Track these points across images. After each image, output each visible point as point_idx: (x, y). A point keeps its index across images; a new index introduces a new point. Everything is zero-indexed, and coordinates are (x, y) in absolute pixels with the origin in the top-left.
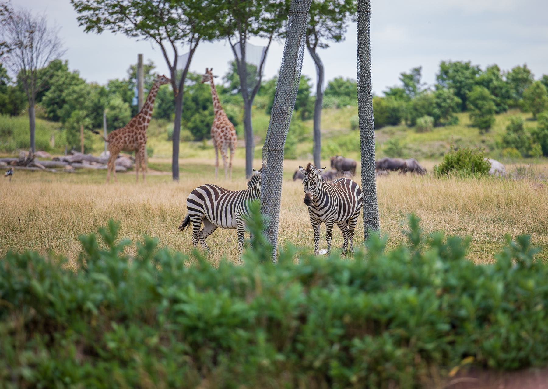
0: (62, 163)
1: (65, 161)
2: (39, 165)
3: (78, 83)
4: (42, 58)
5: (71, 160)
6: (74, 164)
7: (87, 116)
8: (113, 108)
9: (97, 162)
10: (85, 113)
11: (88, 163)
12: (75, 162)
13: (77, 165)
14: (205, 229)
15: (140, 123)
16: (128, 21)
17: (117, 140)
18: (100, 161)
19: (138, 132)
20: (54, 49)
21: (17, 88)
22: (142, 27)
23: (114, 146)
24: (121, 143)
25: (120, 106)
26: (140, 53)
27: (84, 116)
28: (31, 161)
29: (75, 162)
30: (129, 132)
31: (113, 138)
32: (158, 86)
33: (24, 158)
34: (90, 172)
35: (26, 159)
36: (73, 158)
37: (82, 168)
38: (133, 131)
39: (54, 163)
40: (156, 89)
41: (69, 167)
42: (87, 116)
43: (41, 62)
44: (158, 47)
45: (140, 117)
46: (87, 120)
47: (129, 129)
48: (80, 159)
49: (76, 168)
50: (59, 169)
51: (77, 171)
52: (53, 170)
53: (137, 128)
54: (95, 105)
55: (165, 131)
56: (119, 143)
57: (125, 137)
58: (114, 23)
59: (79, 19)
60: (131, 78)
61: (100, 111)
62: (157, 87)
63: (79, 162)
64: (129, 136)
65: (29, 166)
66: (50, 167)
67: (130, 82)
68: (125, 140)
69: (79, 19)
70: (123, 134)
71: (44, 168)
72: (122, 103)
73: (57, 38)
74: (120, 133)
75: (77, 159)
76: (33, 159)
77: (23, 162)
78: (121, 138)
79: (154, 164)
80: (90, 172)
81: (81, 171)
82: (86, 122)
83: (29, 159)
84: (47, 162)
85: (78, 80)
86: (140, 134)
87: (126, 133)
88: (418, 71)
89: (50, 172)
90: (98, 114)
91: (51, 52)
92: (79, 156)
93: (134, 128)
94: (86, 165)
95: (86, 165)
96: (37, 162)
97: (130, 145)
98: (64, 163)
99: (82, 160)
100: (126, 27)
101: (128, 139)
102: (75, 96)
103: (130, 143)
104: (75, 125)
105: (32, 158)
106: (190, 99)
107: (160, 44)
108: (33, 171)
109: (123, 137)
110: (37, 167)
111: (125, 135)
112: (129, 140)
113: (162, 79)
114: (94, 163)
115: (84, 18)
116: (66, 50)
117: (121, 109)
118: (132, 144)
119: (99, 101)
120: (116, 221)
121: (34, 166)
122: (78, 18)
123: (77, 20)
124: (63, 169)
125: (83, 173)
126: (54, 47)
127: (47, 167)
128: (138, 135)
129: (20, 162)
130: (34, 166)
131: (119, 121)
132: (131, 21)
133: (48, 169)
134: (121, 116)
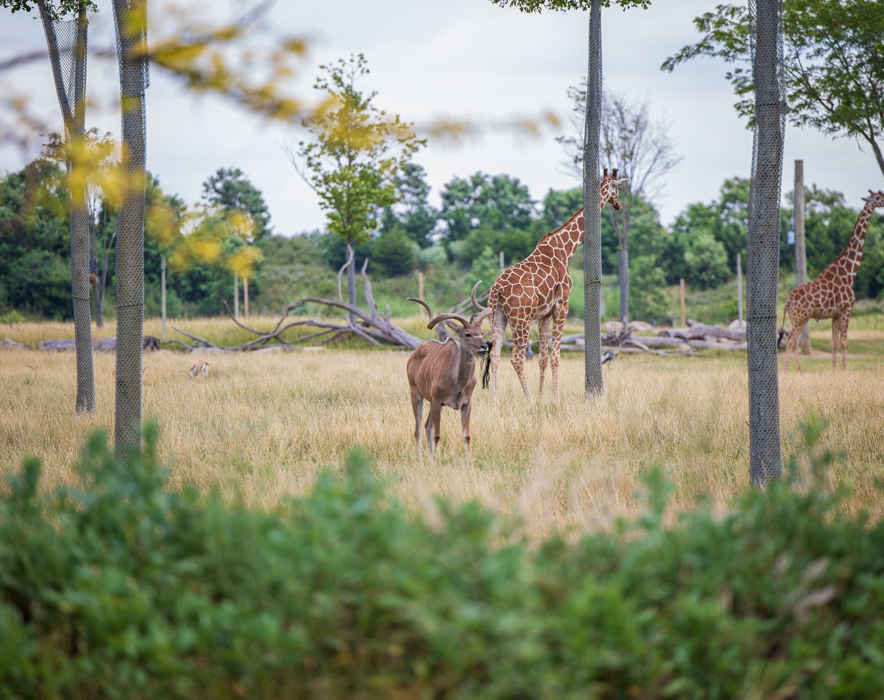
0: (672, 340)
1: (678, 336)
2: (639, 344)
3: (641, 210)
4: (641, 169)
5: (688, 336)
6: (692, 342)
7: (658, 264)
8: (700, 250)
9: (729, 338)
10: (653, 258)
11: (715, 339)
12: (694, 338)
13: (698, 343)
14: (439, 405)
15: (842, 272)
16: (817, 105)
17: (804, 300)
18: (733, 336)
19: (840, 287)
20: (661, 155)
21: (545, 221)
22: (836, 117)
23: (798, 312)
24: (809, 307)
25: (711, 248)
26: (799, 158)
27: (652, 264)
28: (626, 337)
29: (694, 338)
30: (824, 287)
31: (797, 298)
32: (871, 210)
33: (615, 332)
34: (719, 354)
35: (618, 334)
36: (691, 332)
37: (707, 348)
38: (831, 286)
39: (661, 339)
40: (869, 215)
41: (685, 347)
42: (658, 264)
43: (638, 177)
44: (869, 146)
45: (843, 262)
46: (659, 270)
47: (824, 282)
48: (702, 333)
49: (697, 349)
50: (669, 350)
51: (701, 352)
52: (661, 352)
53: (837, 281)
54: (670, 246)
55: (785, 287)
56: (806, 306)
57: (818, 296)
58: (795, 111)
59: (738, 107)
60: (725, 202)
61: (677, 256)
62: (869, 212)
63: (700, 338)
64: (824, 293)
65: (623, 346)
66: (657, 347)
67: (723, 207)
68: (816, 302)
69: (738, 107)
70: (814, 291)
71: (646, 348)
72: (713, 242)
73: (665, 137)
74: (808, 291)
75: (697, 334)
76: (629, 334)
77: (614, 339)
78: (810, 299)
79: (819, 341)
80: (719, 354)
81: (705, 352)
82: (656, 273)
83: (622, 334)
84: (652, 340)
85: (642, 205)
86: (843, 290)
87: (819, 288)
88: (800, 354)
89: (658, 354)
90: (674, 260)
91: (655, 160)
92: (700, 329)
93: (833, 281)
94: (711, 342)
95: (711, 342)
96: (635, 338)
97: (826, 310)
98: (677, 340)
99: (705, 334)
100: (815, 115)
101: (823, 300)
102: (634, 231)
103: (826, 305)
104: (639, 279)
105: (627, 332)
106: (825, 234)
107: (872, 141)
108: (630, 353)
109: (813, 296)
110: (637, 347)
111: (816, 293)
112: (825, 301)
113: (878, 198)
114: (725, 340)
115: (745, 104)
116: (681, 159)
117: (711, 252)
118: (830, 308)
119: (676, 239)
120: (685, 426)
121: (629, 344)
122: (735, 106)
123: (735, 109)
124: (677, 350)
125: (710, 356)
126: (660, 151)
127: (651, 347)
128: (839, 291)
129: (609, 338)
130: (629, 344)
131: (710, 272)
132: (823, 104)
133: (652, 351)
134: (713, 264)
